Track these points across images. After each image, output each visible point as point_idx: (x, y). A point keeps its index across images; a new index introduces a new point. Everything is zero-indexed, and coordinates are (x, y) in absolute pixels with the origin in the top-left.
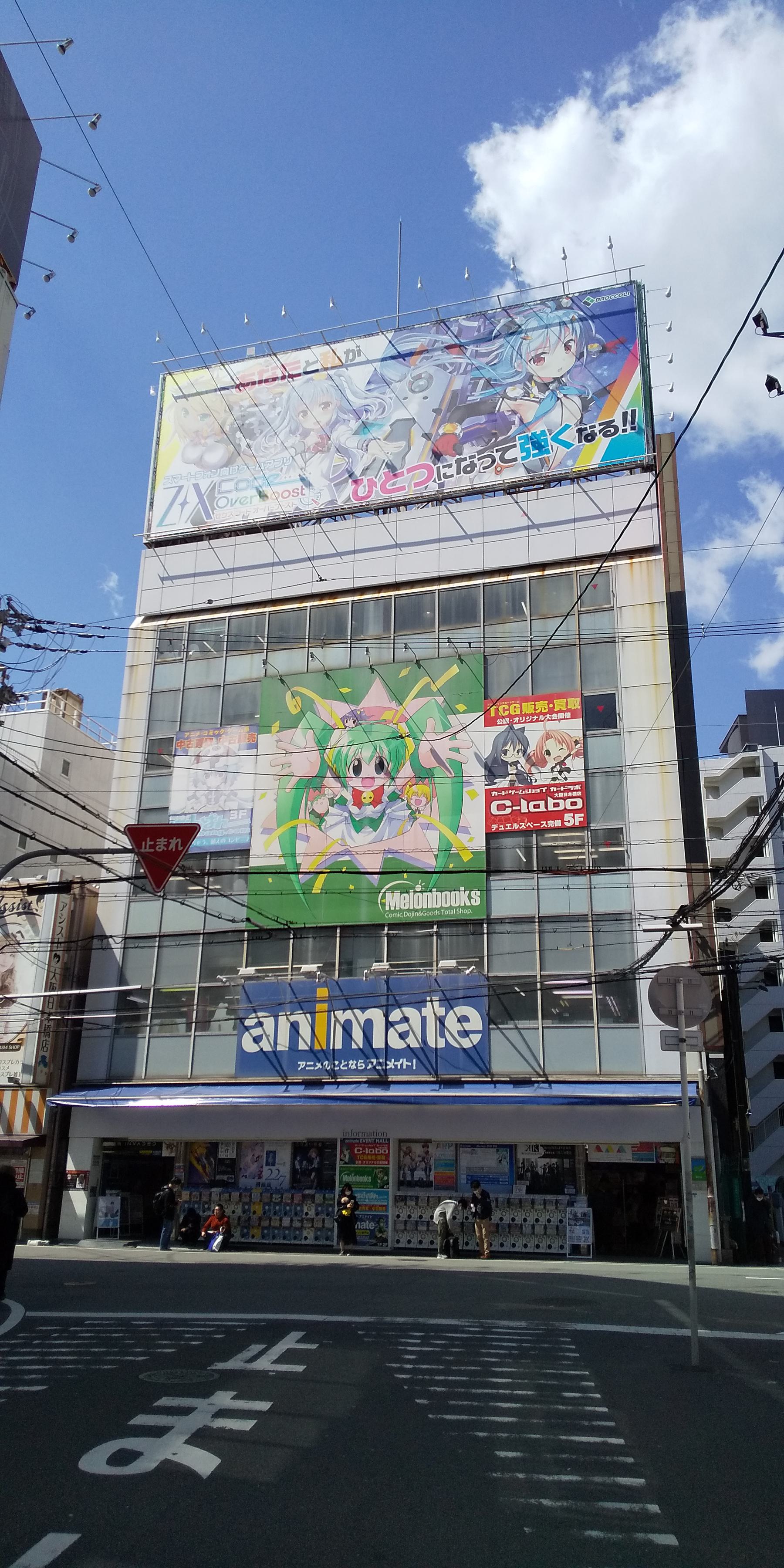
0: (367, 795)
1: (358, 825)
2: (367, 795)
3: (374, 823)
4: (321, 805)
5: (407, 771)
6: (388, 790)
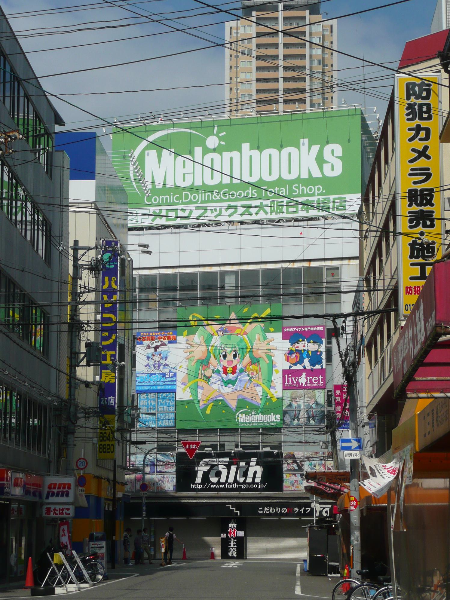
0: (230, 369)
1: (227, 383)
2: (230, 369)
3: (233, 382)
4: (208, 373)
5: (247, 359)
6: (239, 367)
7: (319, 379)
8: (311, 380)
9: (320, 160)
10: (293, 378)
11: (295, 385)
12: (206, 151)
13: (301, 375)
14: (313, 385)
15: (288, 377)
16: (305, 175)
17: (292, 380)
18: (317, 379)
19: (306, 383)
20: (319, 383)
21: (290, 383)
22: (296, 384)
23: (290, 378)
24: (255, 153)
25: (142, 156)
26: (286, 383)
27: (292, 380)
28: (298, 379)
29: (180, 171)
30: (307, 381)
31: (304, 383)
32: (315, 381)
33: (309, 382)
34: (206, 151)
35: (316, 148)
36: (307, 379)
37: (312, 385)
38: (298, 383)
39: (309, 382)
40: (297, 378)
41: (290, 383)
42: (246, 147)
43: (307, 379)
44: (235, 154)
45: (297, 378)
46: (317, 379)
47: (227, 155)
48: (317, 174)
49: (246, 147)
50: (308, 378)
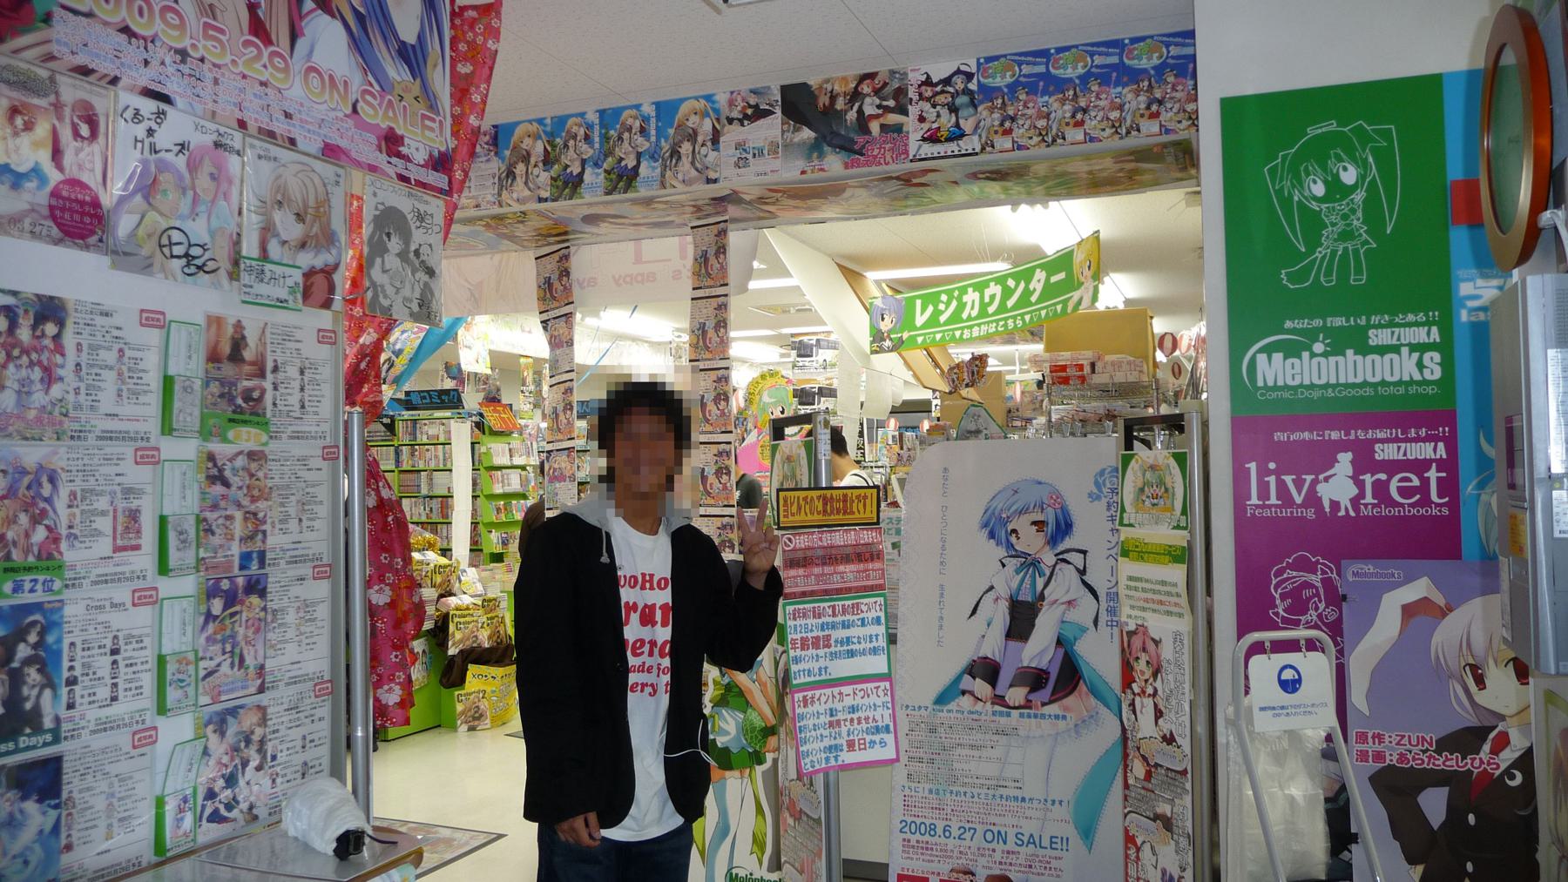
7: (1425, 482)
8: (1381, 490)
9: (1420, 366)
10: (1289, 479)
11: (1298, 513)
12: (1313, 355)
13: (1333, 462)
14: (1395, 512)
15: (1263, 472)
16: (1406, 378)
17: (1281, 485)
18: (1416, 482)
19: (1355, 502)
20: (1426, 501)
21: (1273, 500)
22: (1305, 505)
23: (1272, 479)
24: (1359, 358)
25: (1253, 359)
26: (1254, 500)
27: (1281, 485)
28: (1315, 482)
29: (1289, 372)
30: (1362, 495)
31: (1345, 502)
32: (1404, 492)
33: (1369, 499)
34: (1313, 355)
35: (1416, 355)
36: (1360, 485)
37: (1385, 511)
38: (1313, 499)
39: (1369, 499)
40: (1309, 478)
41: (1273, 500)
42: (1350, 352)
43: (1360, 485)
44: (1340, 358)
45: (1309, 478)
46: (1416, 482)
47: (1332, 359)
48: (1417, 377)
49: (1350, 352)
50: (1368, 479)
